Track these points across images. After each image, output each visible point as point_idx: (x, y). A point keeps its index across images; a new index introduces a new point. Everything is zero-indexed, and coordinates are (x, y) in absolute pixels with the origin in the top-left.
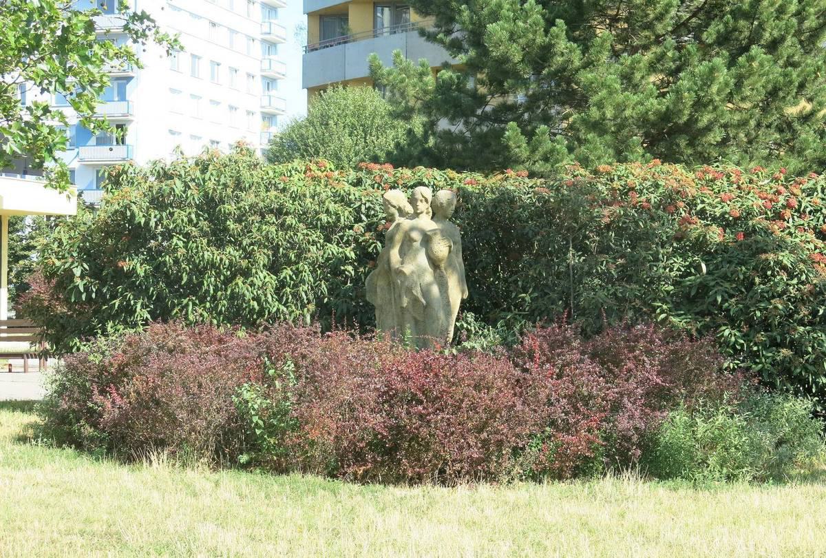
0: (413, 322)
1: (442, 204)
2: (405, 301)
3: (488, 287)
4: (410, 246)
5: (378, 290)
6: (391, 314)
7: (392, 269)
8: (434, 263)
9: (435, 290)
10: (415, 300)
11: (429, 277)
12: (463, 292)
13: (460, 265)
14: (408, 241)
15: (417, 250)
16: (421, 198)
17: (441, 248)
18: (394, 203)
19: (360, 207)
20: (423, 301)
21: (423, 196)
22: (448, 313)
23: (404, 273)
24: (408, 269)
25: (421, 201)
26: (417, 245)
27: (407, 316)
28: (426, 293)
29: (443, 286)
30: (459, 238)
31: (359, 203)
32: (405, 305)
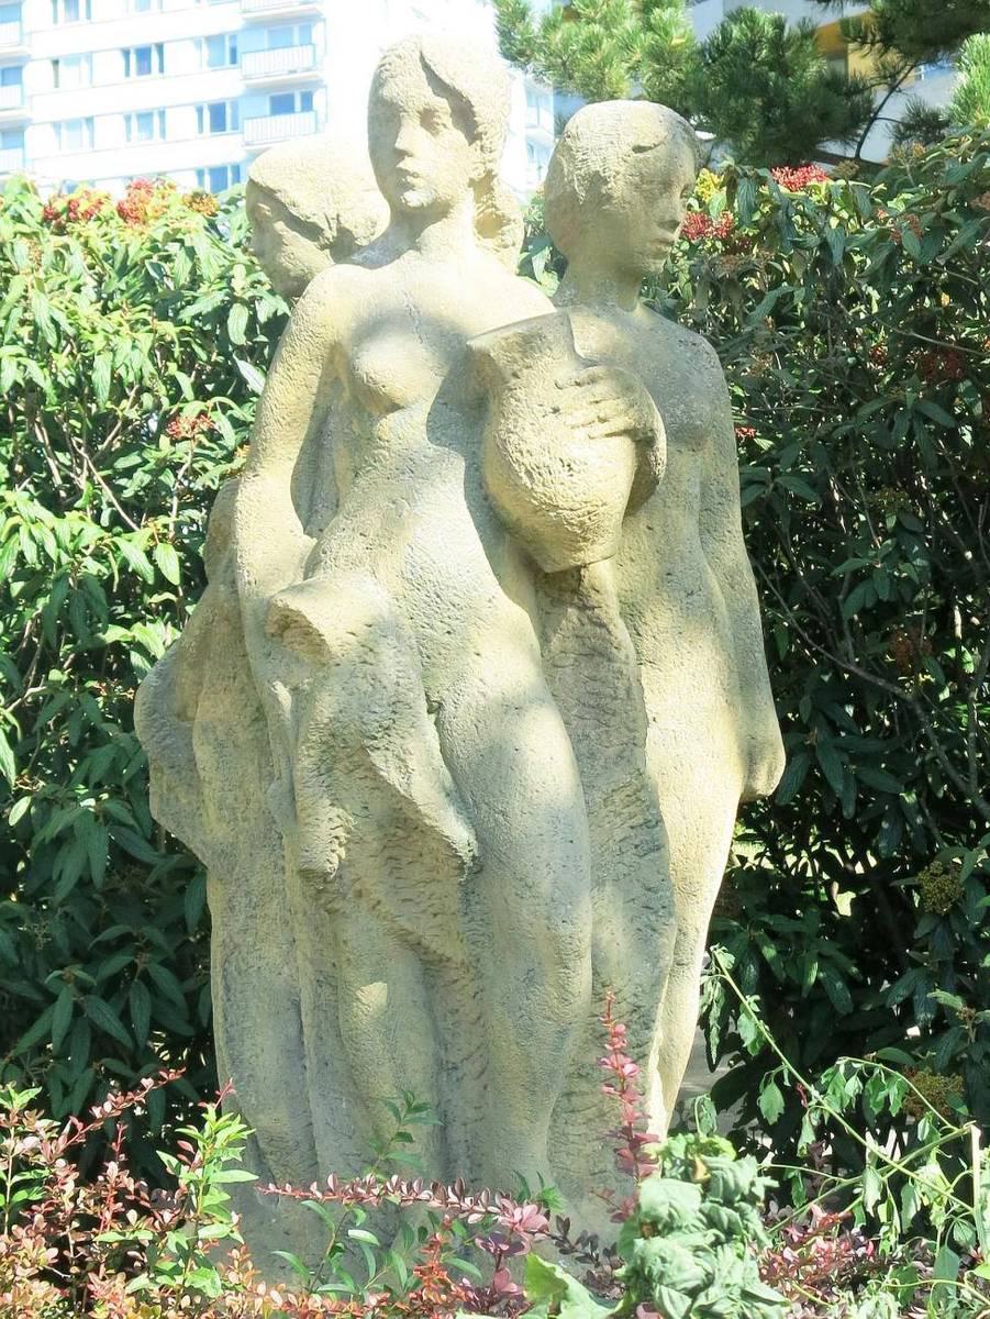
0: (404, 968)
1: (596, 180)
2: (329, 832)
3: (906, 719)
4: (364, 443)
5: (203, 754)
6: (273, 908)
7: (247, 607)
8: (541, 567)
9: (546, 754)
10: (399, 826)
11: (501, 648)
12: (751, 758)
13: (731, 580)
14: (347, 407)
15: (410, 468)
16: (426, 96)
17: (575, 449)
18: (307, 206)
19: (221, 315)
20: (459, 833)
21: (439, 86)
22: (651, 904)
23: (309, 635)
24: (337, 612)
25: (427, 118)
26: (406, 430)
27: (360, 930)
28: (478, 778)
29: (604, 714)
30: (732, 651)
31: (218, 298)
32: (331, 857)
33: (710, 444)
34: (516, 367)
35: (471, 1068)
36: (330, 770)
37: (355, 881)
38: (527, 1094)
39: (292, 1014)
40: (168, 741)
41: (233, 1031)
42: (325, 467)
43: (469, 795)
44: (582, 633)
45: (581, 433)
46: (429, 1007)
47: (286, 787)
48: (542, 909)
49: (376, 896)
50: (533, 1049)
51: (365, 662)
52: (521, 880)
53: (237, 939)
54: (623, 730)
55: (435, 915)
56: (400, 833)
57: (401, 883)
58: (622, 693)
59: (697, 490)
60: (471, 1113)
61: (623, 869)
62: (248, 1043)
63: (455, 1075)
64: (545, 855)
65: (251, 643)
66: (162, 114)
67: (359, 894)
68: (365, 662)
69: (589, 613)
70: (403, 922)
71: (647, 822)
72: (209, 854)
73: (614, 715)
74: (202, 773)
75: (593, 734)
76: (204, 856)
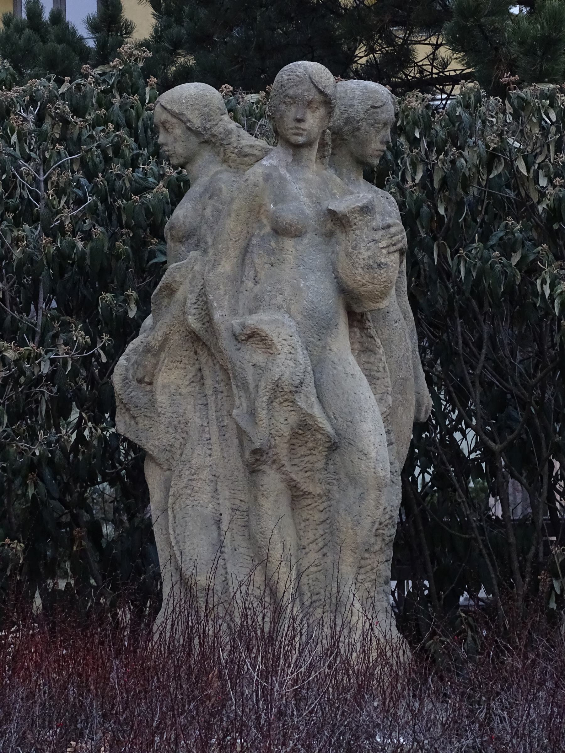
34: (356, 221)
36: (272, 402)
37: (273, 455)
38: (353, 554)
39: (214, 527)
40: (133, 394)
41: (179, 538)
43: (332, 414)
44: (362, 341)
45: (384, 251)
49: (283, 462)
50: (359, 531)
51: (290, 353)
52: (361, 451)
53: (181, 492)
54: (383, 387)
55: (306, 472)
56: (300, 432)
57: (293, 456)
58: (381, 369)
62: (188, 543)
64: (373, 440)
67: (274, 462)
68: (290, 353)
69: (365, 331)
73: (378, 379)
74: (160, 409)
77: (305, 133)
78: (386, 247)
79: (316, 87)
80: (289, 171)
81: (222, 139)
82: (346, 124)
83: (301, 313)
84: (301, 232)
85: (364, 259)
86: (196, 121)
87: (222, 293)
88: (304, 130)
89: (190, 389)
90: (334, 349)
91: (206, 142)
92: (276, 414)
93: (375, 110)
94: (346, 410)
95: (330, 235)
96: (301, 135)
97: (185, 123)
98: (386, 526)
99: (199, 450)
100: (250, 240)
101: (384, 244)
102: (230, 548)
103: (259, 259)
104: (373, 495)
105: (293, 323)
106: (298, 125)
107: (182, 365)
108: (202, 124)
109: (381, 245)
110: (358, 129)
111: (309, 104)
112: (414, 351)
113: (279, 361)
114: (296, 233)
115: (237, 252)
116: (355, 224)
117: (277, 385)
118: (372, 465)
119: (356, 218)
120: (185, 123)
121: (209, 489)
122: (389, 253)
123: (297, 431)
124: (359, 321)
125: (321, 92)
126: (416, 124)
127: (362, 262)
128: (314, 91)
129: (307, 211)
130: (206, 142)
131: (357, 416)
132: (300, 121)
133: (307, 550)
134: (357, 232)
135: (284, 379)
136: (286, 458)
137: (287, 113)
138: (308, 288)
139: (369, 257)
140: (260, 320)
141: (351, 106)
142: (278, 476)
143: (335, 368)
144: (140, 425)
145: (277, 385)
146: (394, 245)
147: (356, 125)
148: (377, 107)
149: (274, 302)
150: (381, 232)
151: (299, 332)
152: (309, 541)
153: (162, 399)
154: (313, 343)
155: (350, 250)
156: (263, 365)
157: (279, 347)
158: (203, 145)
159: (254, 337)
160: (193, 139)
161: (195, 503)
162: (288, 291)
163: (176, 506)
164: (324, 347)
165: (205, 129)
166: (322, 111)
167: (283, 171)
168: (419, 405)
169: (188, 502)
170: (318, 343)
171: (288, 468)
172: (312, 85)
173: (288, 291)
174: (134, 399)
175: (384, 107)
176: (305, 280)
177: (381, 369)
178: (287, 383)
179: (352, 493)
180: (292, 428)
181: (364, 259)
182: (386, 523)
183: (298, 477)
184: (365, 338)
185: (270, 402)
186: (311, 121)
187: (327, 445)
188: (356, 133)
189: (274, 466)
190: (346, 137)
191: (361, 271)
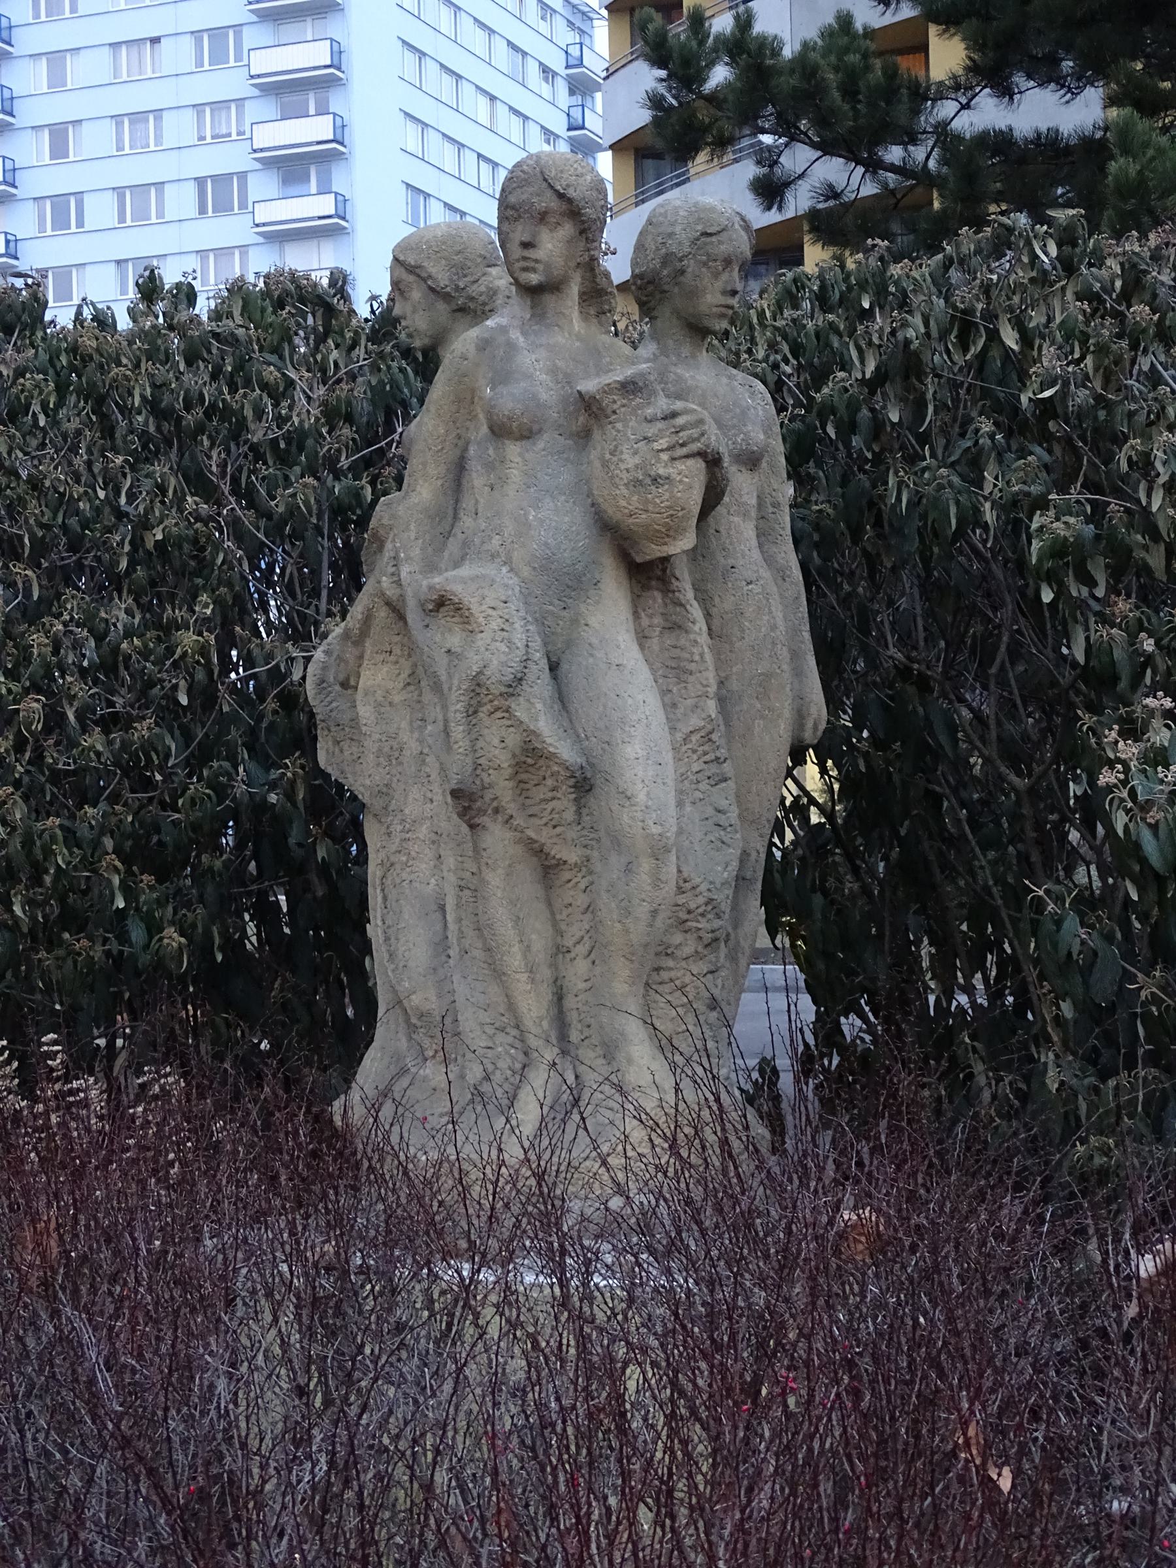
33: (764, 465)
34: (615, 407)
35: (582, 949)
36: (475, 712)
39: (438, 915)
40: (334, 704)
41: (390, 931)
42: (464, 482)
45: (664, 457)
46: (549, 904)
47: (442, 727)
48: (639, 815)
49: (509, 812)
53: (392, 859)
56: (530, 761)
57: (528, 802)
58: (697, 658)
59: (754, 501)
60: (582, 985)
61: (699, 795)
62: (402, 940)
63: (568, 956)
64: (640, 774)
65: (413, 616)
66: (202, 138)
67: (496, 811)
70: (531, 833)
71: (717, 758)
72: (367, 795)
74: (364, 729)
75: (675, 690)
76: (364, 797)
77: (540, 267)
78: (668, 449)
79: (552, 187)
80: (524, 334)
81: (484, 304)
82: (664, 264)
83: (529, 564)
84: (531, 431)
85: (628, 470)
86: (442, 276)
87: (413, 535)
88: (537, 261)
89: (404, 695)
90: (593, 621)
91: (462, 310)
92: (486, 731)
93: (709, 239)
94: (601, 725)
95: (584, 436)
96: (534, 270)
97: (424, 280)
98: (702, 915)
99: (415, 793)
100: (466, 449)
101: (663, 443)
102: (457, 949)
103: (477, 479)
104: (646, 865)
105: (514, 581)
106: (526, 253)
107: (392, 658)
108: (451, 280)
109: (656, 446)
110: (682, 272)
111: (543, 217)
112: (795, 632)
113: (480, 643)
114: (527, 434)
115: (442, 469)
116: (614, 412)
117: (477, 684)
118: (639, 815)
119: (615, 402)
120: (424, 280)
121: (429, 853)
122: (673, 459)
123: (523, 759)
124: (658, 579)
125: (561, 196)
126: (863, 286)
127: (625, 475)
128: (549, 193)
129: (544, 396)
130: (462, 310)
131: (618, 734)
132: (526, 245)
133: (572, 955)
134: (619, 426)
135: (488, 673)
136: (512, 805)
137: (511, 235)
138: (542, 521)
139: (637, 466)
140: (457, 580)
141: (671, 235)
142: (509, 835)
143: (592, 655)
144: (346, 753)
145: (477, 684)
146: (682, 445)
147: (678, 265)
148: (711, 235)
149: (486, 547)
150: (660, 425)
151: (525, 597)
152: (574, 939)
153: (365, 712)
154: (552, 613)
155: (608, 456)
156: (459, 650)
157: (481, 619)
158: (459, 315)
159: (442, 604)
160: (441, 306)
161: (413, 877)
162: (509, 528)
163: (388, 882)
164: (575, 621)
165: (457, 288)
166: (567, 230)
167: (515, 335)
168: (800, 716)
169: (404, 875)
170: (564, 613)
171: (518, 821)
172: (545, 185)
173: (509, 528)
174: (334, 714)
175: (724, 234)
176: (537, 508)
177: (697, 658)
178: (493, 679)
179: (616, 862)
180: (514, 756)
181: (628, 470)
182: (700, 910)
183: (544, 836)
184: (670, 607)
185: (472, 712)
186: (550, 246)
187: (572, 782)
188: (682, 279)
189: (500, 818)
190: (666, 287)
191: (625, 492)
